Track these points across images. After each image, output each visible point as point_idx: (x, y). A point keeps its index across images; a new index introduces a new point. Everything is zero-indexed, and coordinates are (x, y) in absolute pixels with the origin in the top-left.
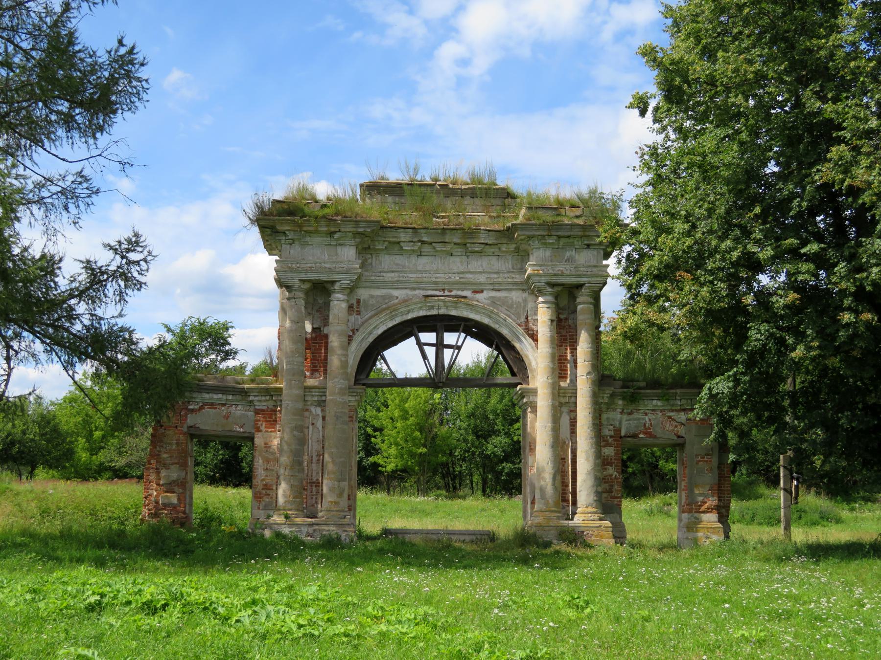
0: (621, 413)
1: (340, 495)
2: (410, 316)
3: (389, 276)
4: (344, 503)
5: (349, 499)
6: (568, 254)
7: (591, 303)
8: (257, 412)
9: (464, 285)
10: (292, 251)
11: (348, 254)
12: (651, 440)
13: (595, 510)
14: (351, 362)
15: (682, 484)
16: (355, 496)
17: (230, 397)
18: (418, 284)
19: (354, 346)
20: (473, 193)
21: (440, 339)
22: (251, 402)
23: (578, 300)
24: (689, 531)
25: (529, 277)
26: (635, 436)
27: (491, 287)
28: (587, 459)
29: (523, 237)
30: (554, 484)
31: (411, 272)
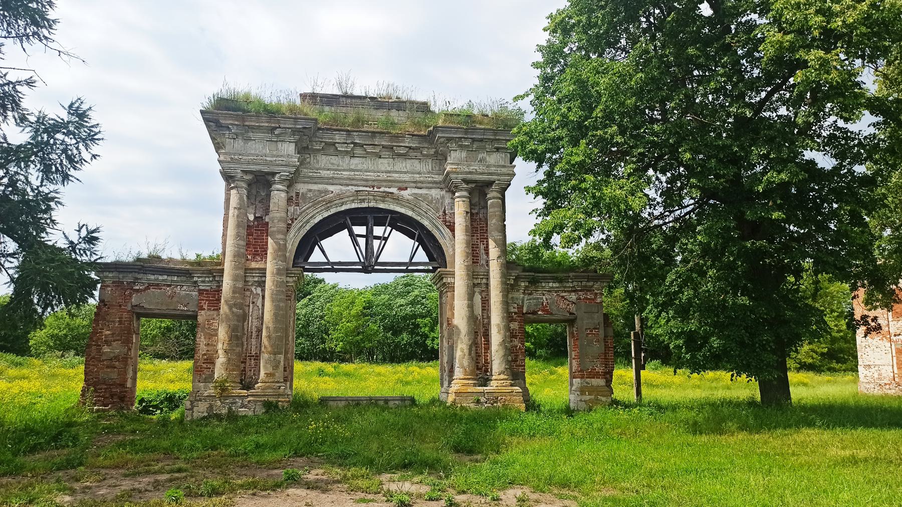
0: (524, 293)
1: (276, 367)
2: (343, 208)
3: (324, 173)
4: (280, 375)
5: (285, 371)
6: (480, 156)
7: (500, 198)
8: (201, 292)
9: (391, 183)
10: (236, 145)
11: (289, 148)
12: (548, 317)
13: (506, 377)
14: (289, 247)
15: (572, 353)
16: (292, 367)
17: (175, 278)
18: (349, 182)
19: (293, 232)
20: (398, 107)
21: (370, 232)
22: (196, 282)
23: (488, 196)
24: (582, 394)
25: (448, 173)
26: (535, 313)
27: (414, 185)
28: (499, 332)
29: (442, 140)
30: (470, 354)
31: (344, 170)
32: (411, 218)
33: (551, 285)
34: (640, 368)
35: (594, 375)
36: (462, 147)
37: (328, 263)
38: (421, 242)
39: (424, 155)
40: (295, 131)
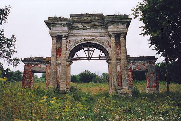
6: (117, 26)
11: (66, 29)
13: (124, 37)
14: (67, 56)
17: (41, 63)
19: (68, 50)
22: (45, 64)
32: (99, 45)
33: (140, 61)
34: (168, 83)
35: (153, 86)
36: (112, 24)
37: (79, 58)
38: (103, 52)
39: (102, 28)
40: (67, 24)
